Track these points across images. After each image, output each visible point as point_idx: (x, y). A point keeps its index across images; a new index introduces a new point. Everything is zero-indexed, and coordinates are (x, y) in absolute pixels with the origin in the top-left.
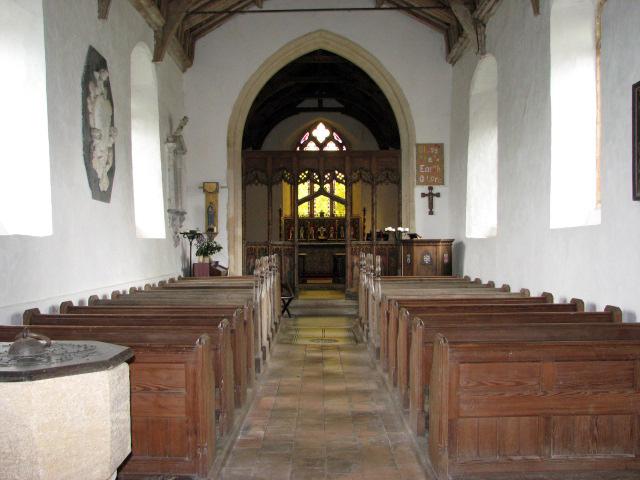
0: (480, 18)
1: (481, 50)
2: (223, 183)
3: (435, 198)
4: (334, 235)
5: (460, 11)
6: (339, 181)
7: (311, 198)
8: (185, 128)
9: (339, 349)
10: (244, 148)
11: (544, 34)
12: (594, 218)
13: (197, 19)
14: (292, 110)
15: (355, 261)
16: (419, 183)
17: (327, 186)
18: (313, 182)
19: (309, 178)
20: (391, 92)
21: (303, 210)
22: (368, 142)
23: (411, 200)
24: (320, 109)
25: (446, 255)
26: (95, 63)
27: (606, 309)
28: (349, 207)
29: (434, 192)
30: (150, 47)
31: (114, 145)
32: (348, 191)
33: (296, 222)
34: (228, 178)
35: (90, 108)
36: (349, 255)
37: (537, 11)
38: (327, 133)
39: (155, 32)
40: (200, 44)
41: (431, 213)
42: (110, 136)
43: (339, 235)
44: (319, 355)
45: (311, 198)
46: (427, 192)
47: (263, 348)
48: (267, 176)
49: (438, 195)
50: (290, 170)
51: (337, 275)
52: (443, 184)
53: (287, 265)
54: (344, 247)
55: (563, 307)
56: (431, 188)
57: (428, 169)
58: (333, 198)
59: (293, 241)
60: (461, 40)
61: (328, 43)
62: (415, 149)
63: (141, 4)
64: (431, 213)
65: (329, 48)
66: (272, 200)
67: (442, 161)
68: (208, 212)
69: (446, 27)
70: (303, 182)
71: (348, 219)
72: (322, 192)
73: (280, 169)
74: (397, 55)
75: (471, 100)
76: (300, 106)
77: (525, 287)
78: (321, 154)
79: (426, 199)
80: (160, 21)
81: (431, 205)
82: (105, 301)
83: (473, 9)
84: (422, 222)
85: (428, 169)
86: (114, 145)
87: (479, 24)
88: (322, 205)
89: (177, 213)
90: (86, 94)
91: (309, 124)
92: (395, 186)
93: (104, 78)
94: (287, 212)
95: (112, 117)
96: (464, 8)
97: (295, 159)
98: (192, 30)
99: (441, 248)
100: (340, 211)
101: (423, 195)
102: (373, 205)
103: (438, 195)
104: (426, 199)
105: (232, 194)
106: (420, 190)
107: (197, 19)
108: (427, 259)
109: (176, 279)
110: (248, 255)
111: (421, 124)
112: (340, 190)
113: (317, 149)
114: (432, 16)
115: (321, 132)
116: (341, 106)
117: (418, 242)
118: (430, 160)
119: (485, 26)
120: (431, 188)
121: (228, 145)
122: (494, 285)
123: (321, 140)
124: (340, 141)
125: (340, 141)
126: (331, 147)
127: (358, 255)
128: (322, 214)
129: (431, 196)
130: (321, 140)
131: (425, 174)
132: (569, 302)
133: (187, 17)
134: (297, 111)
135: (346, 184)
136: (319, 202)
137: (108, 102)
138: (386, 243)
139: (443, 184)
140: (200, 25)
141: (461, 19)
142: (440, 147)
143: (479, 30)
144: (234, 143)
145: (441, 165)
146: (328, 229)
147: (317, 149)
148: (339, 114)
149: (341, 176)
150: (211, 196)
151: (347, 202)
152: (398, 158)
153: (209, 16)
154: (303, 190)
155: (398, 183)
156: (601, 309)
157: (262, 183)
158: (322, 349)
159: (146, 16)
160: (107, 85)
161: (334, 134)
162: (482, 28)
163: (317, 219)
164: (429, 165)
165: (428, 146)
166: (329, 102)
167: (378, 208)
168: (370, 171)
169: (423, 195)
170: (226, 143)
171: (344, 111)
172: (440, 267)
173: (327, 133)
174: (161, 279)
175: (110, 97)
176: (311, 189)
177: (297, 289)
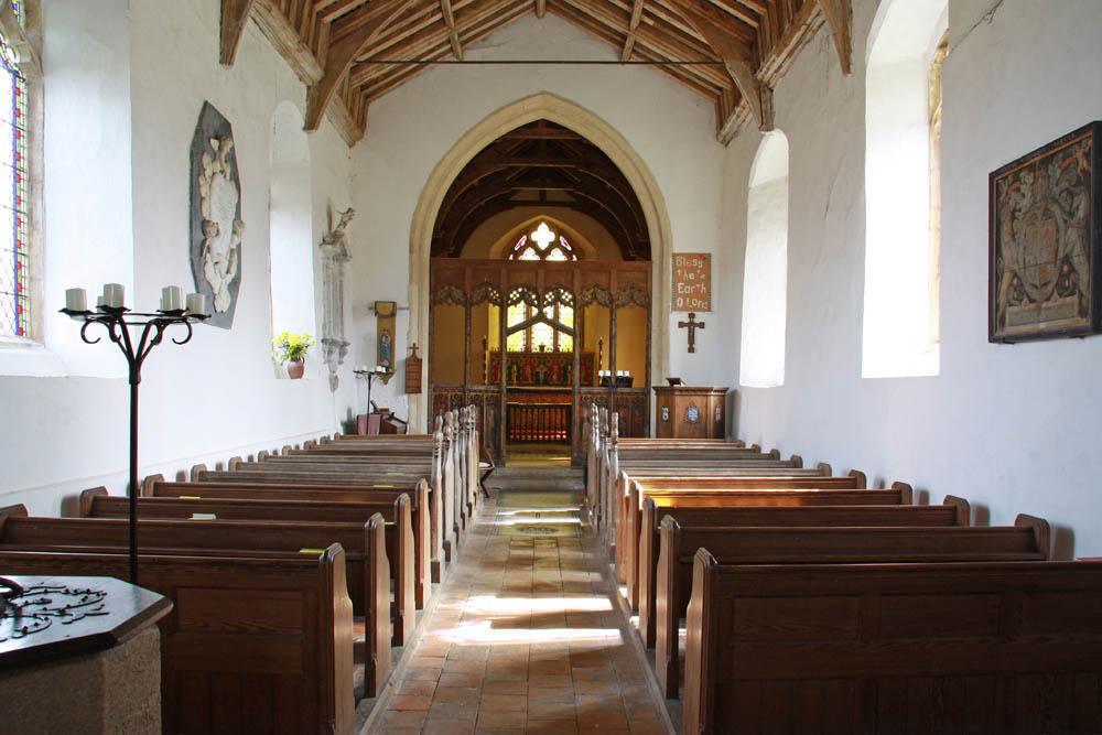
0: (766, 80)
1: (767, 123)
2: (402, 302)
3: (697, 329)
4: (559, 379)
5: (736, 69)
6: (566, 304)
7: (526, 326)
8: (349, 224)
9: (557, 543)
10: (433, 254)
11: (858, 97)
13: (372, 73)
14: (505, 204)
15: (585, 415)
16: (675, 309)
17: (549, 312)
18: (529, 304)
19: (523, 297)
20: (640, 181)
21: (516, 343)
22: (603, 248)
23: (663, 332)
25: (718, 410)
26: (212, 133)
27: (946, 501)
28: (578, 340)
29: (697, 321)
30: (300, 110)
31: (239, 246)
32: (579, 317)
33: (505, 359)
34: (410, 299)
35: (204, 191)
36: (577, 407)
37: (846, 68)
38: (551, 237)
39: (309, 87)
40: (375, 107)
42: (234, 232)
43: (564, 377)
44: (529, 553)
45: (526, 326)
46: (687, 320)
47: (447, 546)
48: (465, 294)
49: (702, 325)
50: (497, 288)
51: (563, 434)
52: (709, 310)
53: (491, 419)
54: (569, 393)
55: (879, 495)
56: (692, 316)
57: (689, 289)
58: (557, 327)
59: (499, 385)
60: (737, 110)
61: (553, 111)
64: (691, 350)
66: (474, 329)
68: (380, 342)
70: (515, 303)
72: (541, 318)
73: (480, 286)
74: (638, 120)
75: (751, 194)
76: (513, 198)
77: (825, 461)
78: (543, 264)
79: (686, 329)
82: (219, 474)
83: (756, 67)
84: (677, 361)
85: (689, 289)
86: (239, 246)
88: (542, 336)
89: (333, 342)
90: (196, 171)
93: (226, 149)
94: (494, 344)
95: (238, 206)
96: (744, 66)
97: (504, 272)
98: (363, 88)
99: (713, 400)
100: (566, 343)
101: (681, 325)
102: (612, 338)
103: (702, 325)
104: (686, 329)
105: (415, 319)
106: (676, 317)
107: (372, 73)
108: (693, 414)
109: (332, 438)
110: (435, 403)
111: (680, 226)
112: (567, 316)
113: (537, 258)
115: (543, 235)
117: (681, 390)
120: (692, 316)
121: (411, 251)
122: (779, 454)
123: (543, 245)
124: (570, 249)
125: (570, 249)
126: (557, 256)
127: (589, 407)
128: (542, 347)
130: (543, 245)
131: (685, 296)
132: (888, 487)
133: (354, 70)
134: (511, 205)
135: (574, 307)
136: (536, 330)
137: (232, 186)
138: (627, 390)
139: (709, 310)
140: (376, 81)
141: (738, 81)
142: (705, 258)
143: (763, 94)
145: (710, 281)
146: (551, 369)
147: (537, 258)
149: (567, 296)
150: (385, 321)
151: (578, 333)
152: (648, 273)
153: (389, 67)
154: (516, 314)
155: (648, 307)
156: (937, 500)
157: (458, 302)
158: (532, 544)
159: (295, 65)
160: (232, 159)
161: (561, 238)
162: (768, 93)
164: (689, 282)
165: (690, 256)
166: (554, 192)
167: (619, 340)
168: (609, 289)
169: (681, 325)
170: (408, 248)
172: (711, 426)
173: (551, 237)
174: (310, 438)
175: (235, 178)
176: (528, 313)
177: (504, 453)
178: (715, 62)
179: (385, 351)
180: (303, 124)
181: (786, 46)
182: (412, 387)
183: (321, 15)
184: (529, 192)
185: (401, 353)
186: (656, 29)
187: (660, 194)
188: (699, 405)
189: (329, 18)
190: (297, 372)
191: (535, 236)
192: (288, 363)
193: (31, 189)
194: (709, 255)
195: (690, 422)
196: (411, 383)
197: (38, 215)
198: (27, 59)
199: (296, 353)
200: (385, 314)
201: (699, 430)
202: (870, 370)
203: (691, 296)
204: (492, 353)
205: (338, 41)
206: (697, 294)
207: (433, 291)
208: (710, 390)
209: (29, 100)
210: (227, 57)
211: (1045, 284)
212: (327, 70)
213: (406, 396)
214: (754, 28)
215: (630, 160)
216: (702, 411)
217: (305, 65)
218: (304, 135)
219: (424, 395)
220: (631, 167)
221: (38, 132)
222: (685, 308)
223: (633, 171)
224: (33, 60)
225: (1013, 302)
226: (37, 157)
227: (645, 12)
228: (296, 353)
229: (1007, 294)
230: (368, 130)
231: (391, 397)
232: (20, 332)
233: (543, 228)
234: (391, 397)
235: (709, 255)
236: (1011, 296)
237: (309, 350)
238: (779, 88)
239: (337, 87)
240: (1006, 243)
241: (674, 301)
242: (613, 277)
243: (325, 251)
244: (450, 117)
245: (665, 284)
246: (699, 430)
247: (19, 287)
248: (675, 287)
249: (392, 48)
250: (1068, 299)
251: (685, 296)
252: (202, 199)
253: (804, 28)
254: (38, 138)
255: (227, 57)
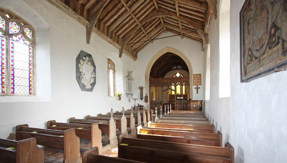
2: (144, 87)
5: (199, 31)
6: (173, 86)
12: (91, 87)
16: (194, 85)
23: (192, 90)
24: (177, 69)
29: (198, 87)
34: (145, 86)
36: (175, 104)
38: (179, 75)
40: (139, 54)
41: (197, 93)
46: (196, 87)
49: (199, 88)
54: (174, 101)
56: (197, 86)
57: (197, 81)
62: (193, 76)
63: (110, 42)
64: (197, 93)
65: (170, 52)
67: (201, 79)
69: (201, 40)
71: (175, 95)
75: (207, 60)
79: (196, 89)
80: (120, 47)
81: (197, 91)
85: (197, 81)
87: (206, 35)
91: (176, 72)
92: (188, 86)
99: (199, 103)
101: (195, 88)
103: (199, 88)
104: (196, 89)
108: (194, 106)
111: (195, 69)
114: (196, 38)
116: (182, 68)
118: (197, 78)
119: (208, 35)
120: (197, 86)
128: (178, 94)
129: (197, 88)
135: (174, 86)
142: (200, 75)
143: (206, 36)
144: (147, 77)
145: (200, 79)
148: (182, 70)
149: (173, 84)
157: (154, 86)
159: (114, 45)
162: (207, 36)
163: (180, 95)
164: (197, 80)
165: (197, 75)
166: (179, 67)
169: (195, 88)
171: (182, 69)
173: (179, 75)
178: (193, 32)
179: (142, 95)
180: (119, 56)
181: (208, 22)
182: (146, 101)
183: (118, 36)
184: (175, 67)
185: (144, 95)
186: (185, 29)
187: (190, 63)
188: (196, 104)
189: (121, 37)
190: (120, 99)
191: (176, 75)
192: (118, 98)
193: (33, 67)
194: (201, 74)
195: (194, 107)
196: (146, 100)
197: (35, 72)
198: (31, 43)
199: (119, 96)
200: (141, 89)
201: (196, 109)
202: (221, 96)
203: (197, 82)
204: (169, 95)
205: (124, 41)
206: (198, 82)
207: (150, 84)
208: (198, 101)
209: (33, 50)
210: (88, 42)
211: (262, 47)
212: (122, 46)
213: (145, 103)
214: (203, 21)
215: (184, 57)
216: (197, 105)
217: (116, 45)
218: (119, 58)
219: (149, 103)
220: (184, 58)
221: (34, 56)
222: (196, 85)
223: (185, 59)
224: (32, 43)
225: (250, 62)
226: (34, 61)
227: (182, 25)
228: (119, 96)
229: (247, 60)
230: (137, 59)
231: (142, 103)
232: (30, 93)
233: (178, 73)
234: (142, 103)
235: (201, 74)
236: (248, 60)
237: (121, 96)
238: (209, 33)
239: (124, 48)
240: (246, 38)
241: (194, 83)
242: (182, 80)
243: (126, 78)
244: (151, 54)
245: (192, 80)
246: (196, 109)
247: (30, 85)
248: (194, 81)
249: (143, 44)
250: (275, 49)
251: (196, 82)
252: (80, 68)
253: (210, 14)
254: (35, 58)
255: (88, 42)
